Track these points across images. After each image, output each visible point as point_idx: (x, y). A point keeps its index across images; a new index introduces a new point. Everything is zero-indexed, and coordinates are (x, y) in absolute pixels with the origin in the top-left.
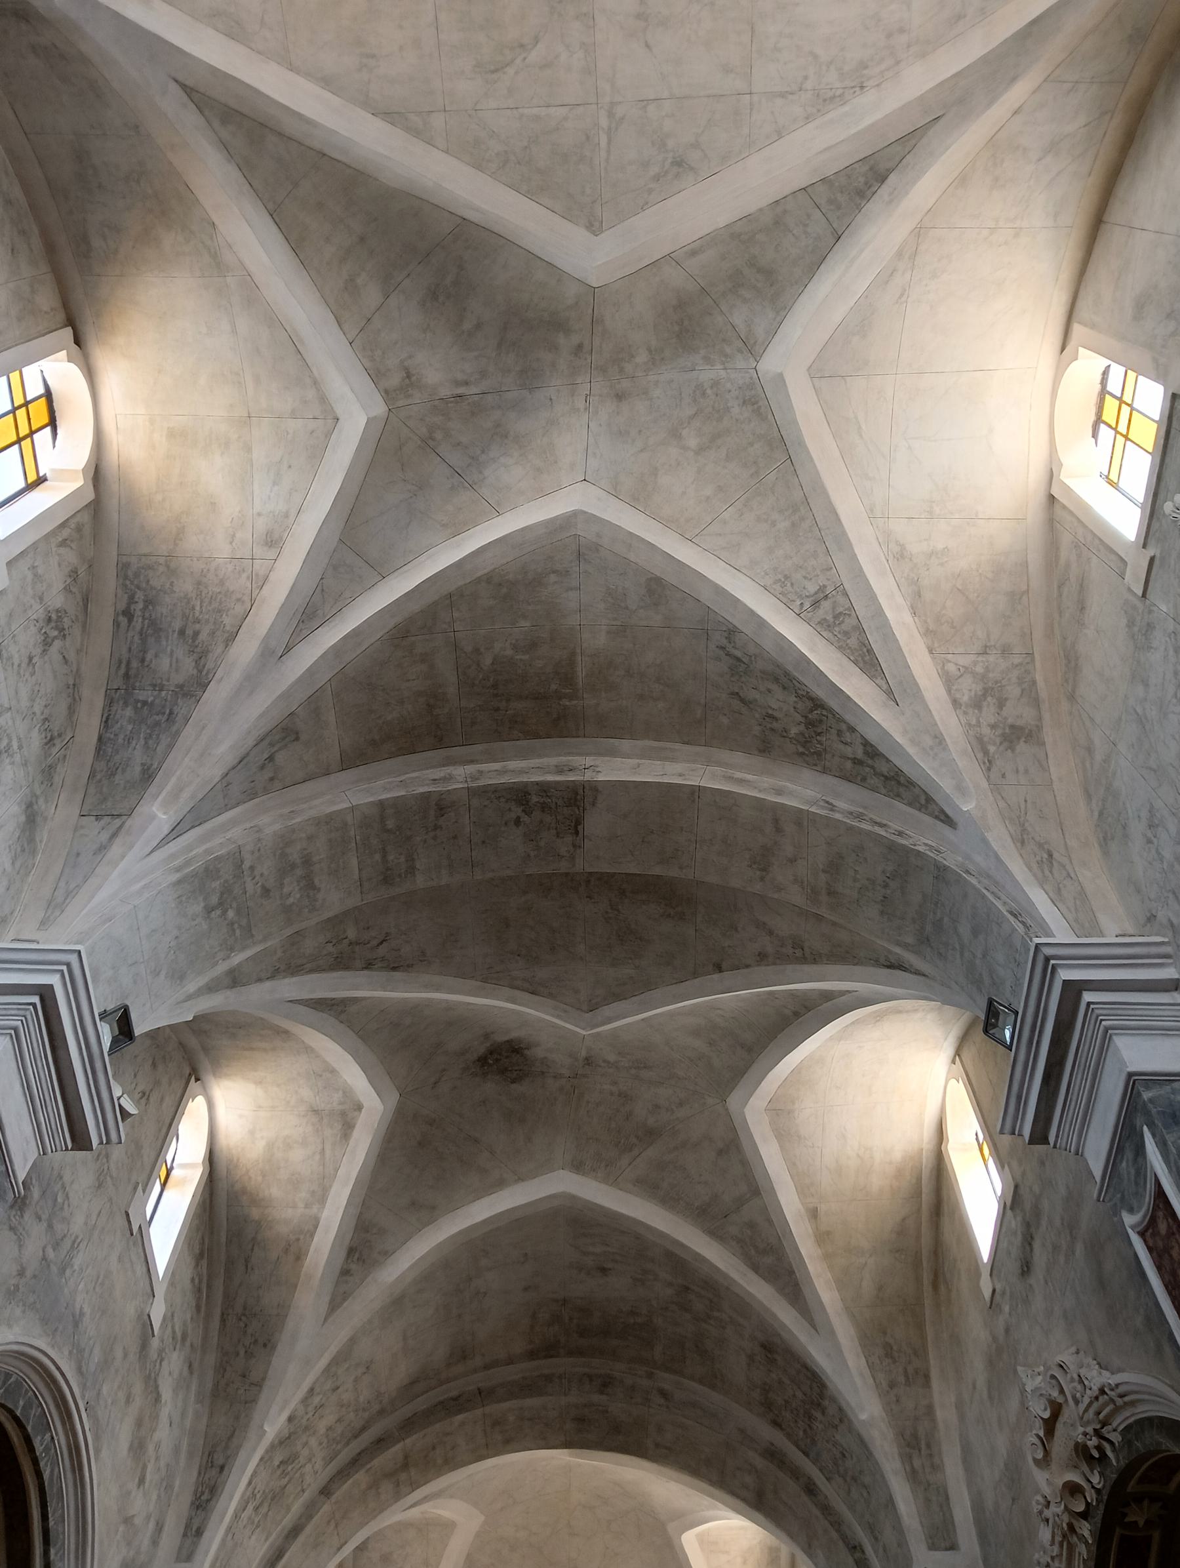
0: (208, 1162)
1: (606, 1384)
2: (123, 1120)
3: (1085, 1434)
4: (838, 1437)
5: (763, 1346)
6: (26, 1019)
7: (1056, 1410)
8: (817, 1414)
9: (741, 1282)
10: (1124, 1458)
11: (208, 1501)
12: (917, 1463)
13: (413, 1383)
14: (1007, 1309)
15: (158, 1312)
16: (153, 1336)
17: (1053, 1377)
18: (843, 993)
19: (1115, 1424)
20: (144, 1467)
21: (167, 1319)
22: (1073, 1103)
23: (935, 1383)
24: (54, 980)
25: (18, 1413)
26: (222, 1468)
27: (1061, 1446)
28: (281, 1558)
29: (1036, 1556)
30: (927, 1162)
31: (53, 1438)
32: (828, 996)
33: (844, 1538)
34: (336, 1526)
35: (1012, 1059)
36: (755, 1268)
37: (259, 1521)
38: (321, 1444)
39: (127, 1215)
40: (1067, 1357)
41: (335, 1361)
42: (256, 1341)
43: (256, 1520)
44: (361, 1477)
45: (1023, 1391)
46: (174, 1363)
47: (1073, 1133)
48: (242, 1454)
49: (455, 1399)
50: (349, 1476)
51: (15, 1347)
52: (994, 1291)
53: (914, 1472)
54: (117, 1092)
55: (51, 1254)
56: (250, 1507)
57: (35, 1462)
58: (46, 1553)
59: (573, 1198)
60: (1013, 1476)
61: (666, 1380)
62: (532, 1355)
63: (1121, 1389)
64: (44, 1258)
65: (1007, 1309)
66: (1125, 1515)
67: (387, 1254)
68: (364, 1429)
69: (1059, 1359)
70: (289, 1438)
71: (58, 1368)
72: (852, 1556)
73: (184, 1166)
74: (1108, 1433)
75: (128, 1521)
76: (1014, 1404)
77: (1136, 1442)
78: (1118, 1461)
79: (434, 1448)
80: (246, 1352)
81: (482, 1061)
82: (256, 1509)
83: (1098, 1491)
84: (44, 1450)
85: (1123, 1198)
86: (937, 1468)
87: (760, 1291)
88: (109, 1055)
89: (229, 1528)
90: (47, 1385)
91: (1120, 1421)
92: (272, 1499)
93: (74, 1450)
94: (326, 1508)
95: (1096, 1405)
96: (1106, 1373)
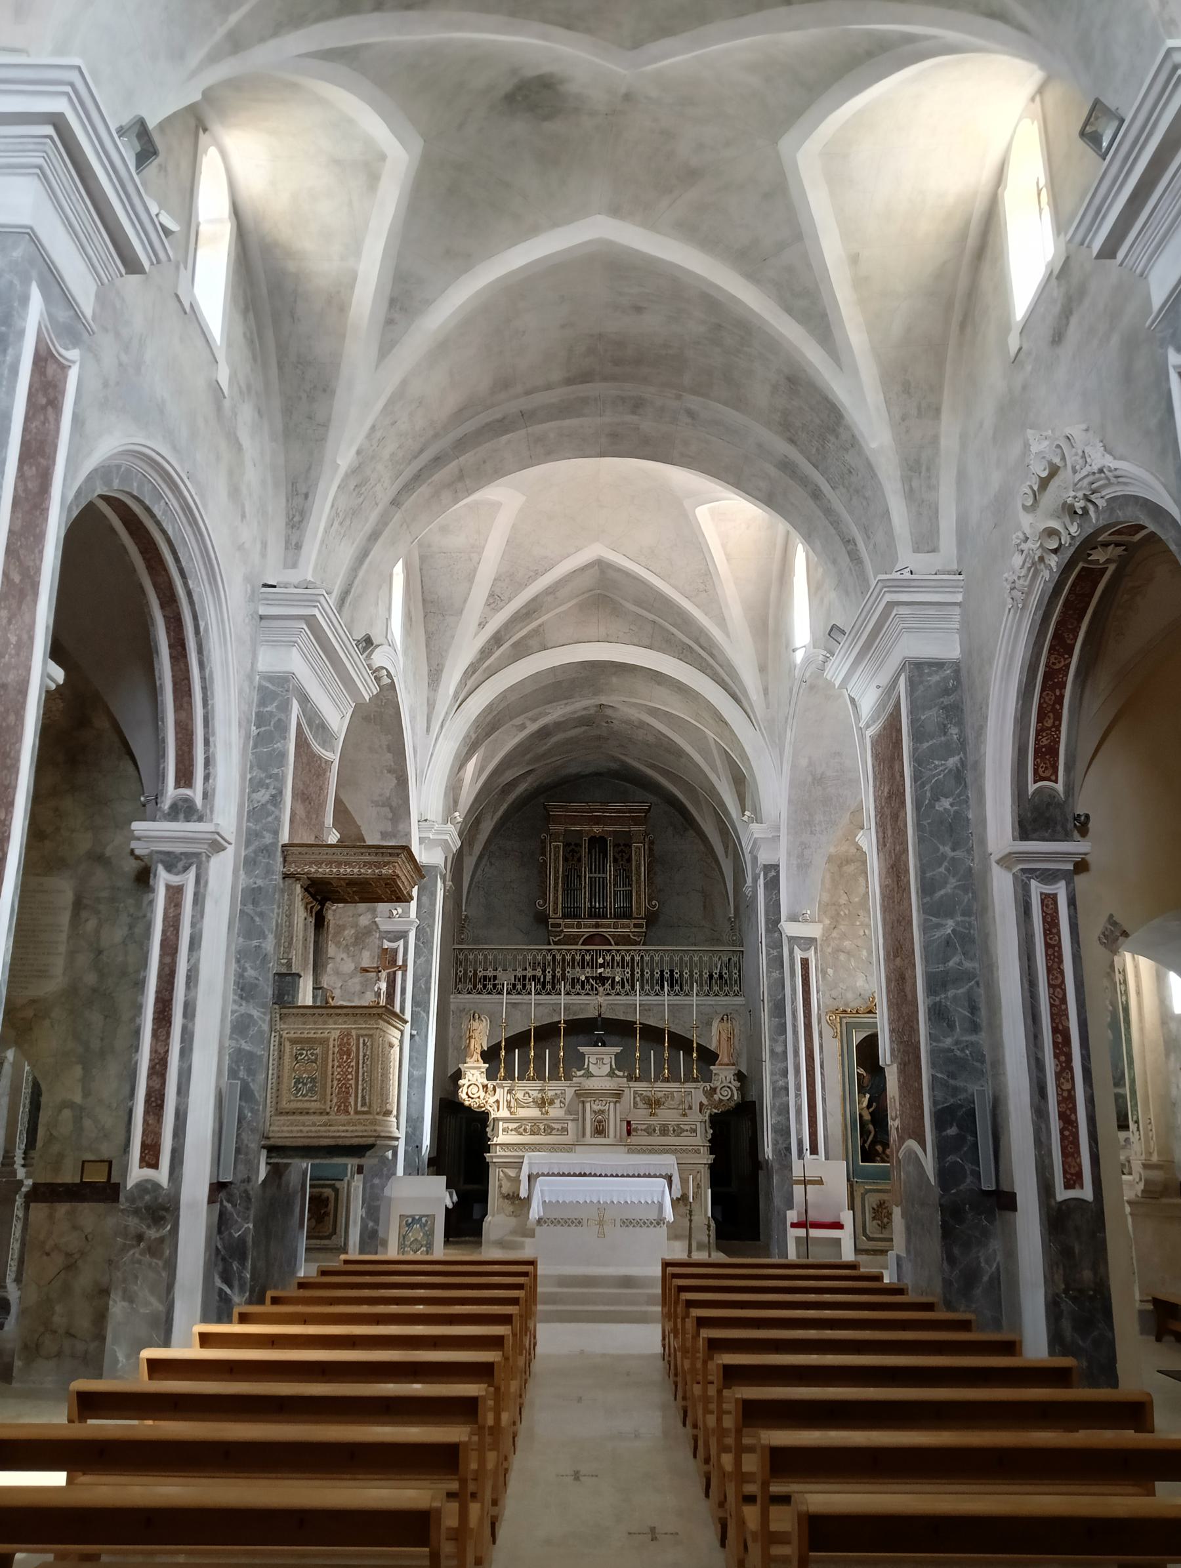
0: (233, 215)
1: (637, 405)
2: (166, 236)
3: (1075, 497)
4: (847, 457)
5: (789, 379)
6: (47, 154)
7: (1054, 471)
8: (832, 439)
9: (772, 322)
10: (1103, 519)
11: (301, 522)
12: (915, 484)
13: (460, 411)
14: (1029, 368)
15: (223, 375)
16: (225, 397)
17: (1058, 446)
18: (927, 38)
19: (1103, 493)
20: (243, 506)
21: (233, 378)
22: (1150, 231)
23: (945, 416)
24: (59, 105)
25: (135, 493)
26: (306, 496)
27: (1051, 498)
28: (367, 556)
29: (1006, 575)
30: (979, 207)
31: (167, 503)
32: (910, 39)
33: (841, 534)
34: (408, 527)
35: (1103, 170)
36: (789, 310)
37: (345, 532)
38: (386, 467)
39: (177, 296)
40: (1076, 431)
41: (391, 402)
42: (315, 387)
43: (343, 531)
44: (424, 490)
45: (1027, 445)
46: (246, 413)
47: (1145, 254)
48: (322, 485)
49: (501, 420)
50: (413, 490)
51: (121, 449)
52: (1020, 349)
53: (911, 490)
54: (154, 210)
55: (124, 358)
56: (336, 524)
57: (158, 523)
58: (186, 584)
59: (610, 243)
60: (1000, 506)
61: (693, 402)
62: (569, 381)
63: (1117, 473)
64: (120, 364)
65: (1029, 368)
66: (1090, 555)
67: (428, 302)
68: (421, 451)
69: (1068, 431)
70: (359, 467)
71: (163, 458)
72: (846, 548)
73: (211, 221)
74: (1096, 498)
75: (241, 548)
76: (1016, 450)
77: (1118, 511)
78: (1097, 520)
79: (484, 462)
80: (308, 396)
81: (510, 98)
82: (341, 524)
83: (1073, 538)
84: (163, 514)
85: (1173, 335)
86: (933, 488)
87: (790, 331)
88: (138, 174)
89: (323, 542)
90: (152, 467)
91: (1109, 492)
92: (353, 515)
93: (187, 509)
94: (398, 516)
95: (1091, 478)
96: (1109, 458)
